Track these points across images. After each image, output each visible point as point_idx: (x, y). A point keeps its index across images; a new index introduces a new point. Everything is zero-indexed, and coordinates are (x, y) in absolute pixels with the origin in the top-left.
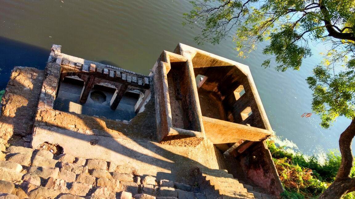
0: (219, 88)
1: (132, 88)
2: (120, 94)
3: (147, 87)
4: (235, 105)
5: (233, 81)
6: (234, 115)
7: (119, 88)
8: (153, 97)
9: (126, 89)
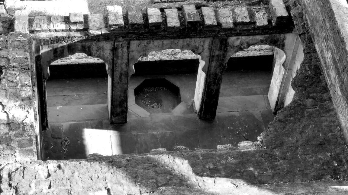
1: (242, 44)
7: (206, 53)
8: (310, 52)
9: (226, 50)
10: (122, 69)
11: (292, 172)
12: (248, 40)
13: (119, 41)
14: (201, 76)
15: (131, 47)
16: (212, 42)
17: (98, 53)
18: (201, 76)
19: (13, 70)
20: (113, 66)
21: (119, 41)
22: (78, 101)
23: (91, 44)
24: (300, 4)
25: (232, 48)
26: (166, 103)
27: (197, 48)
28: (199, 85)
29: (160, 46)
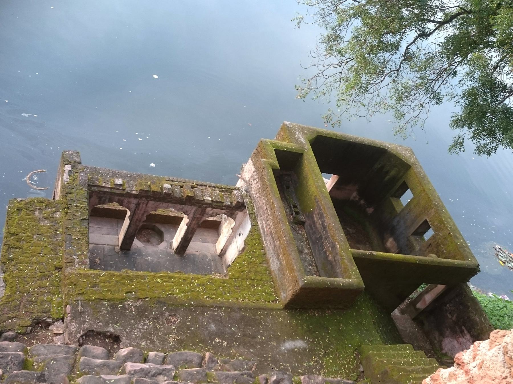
0: (362, 194)
1: (213, 213)
2: (192, 225)
3: (241, 206)
4: (396, 220)
5: (387, 178)
6: (396, 240)
8: (254, 225)
9: (203, 215)
10: (139, 217)
11: (134, 305)
12: (217, 212)
13: (143, 200)
14: (127, 222)
15: (148, 204)
16: (197, 209)
17: (127, 205)
18: (127, 222)
19: (77, 208)
20: (133, 214)
21: (143, 200)
22: (99, 231)
23: (125, 199)
24: (250, 197)
25: (207, 214)
26: (154, 240)
27: (187, 212)
28: (180, 233)
29: (166, 207)
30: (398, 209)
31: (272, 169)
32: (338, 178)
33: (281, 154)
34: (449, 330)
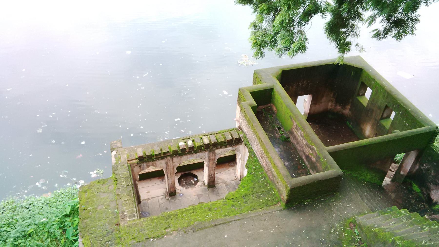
10: (171, 171)
29: (186, 158)
30: (365, 104)
31: (251, 107)
32: (312, 96)
33: (256, 95)
34: (432, 184)
